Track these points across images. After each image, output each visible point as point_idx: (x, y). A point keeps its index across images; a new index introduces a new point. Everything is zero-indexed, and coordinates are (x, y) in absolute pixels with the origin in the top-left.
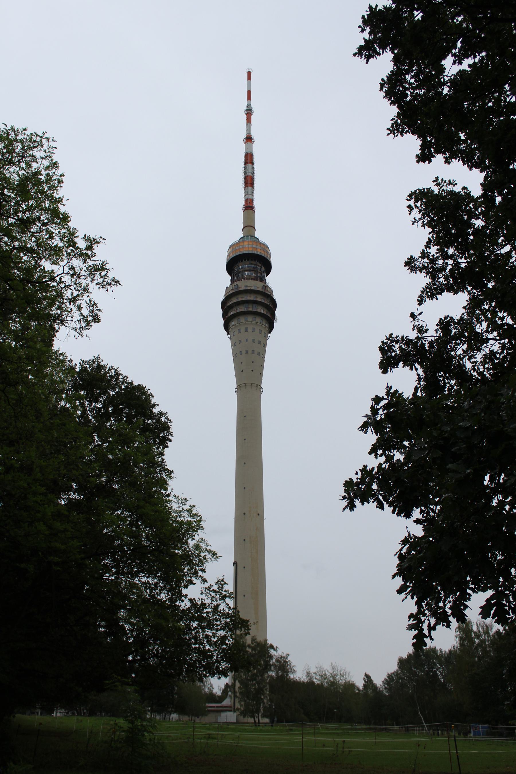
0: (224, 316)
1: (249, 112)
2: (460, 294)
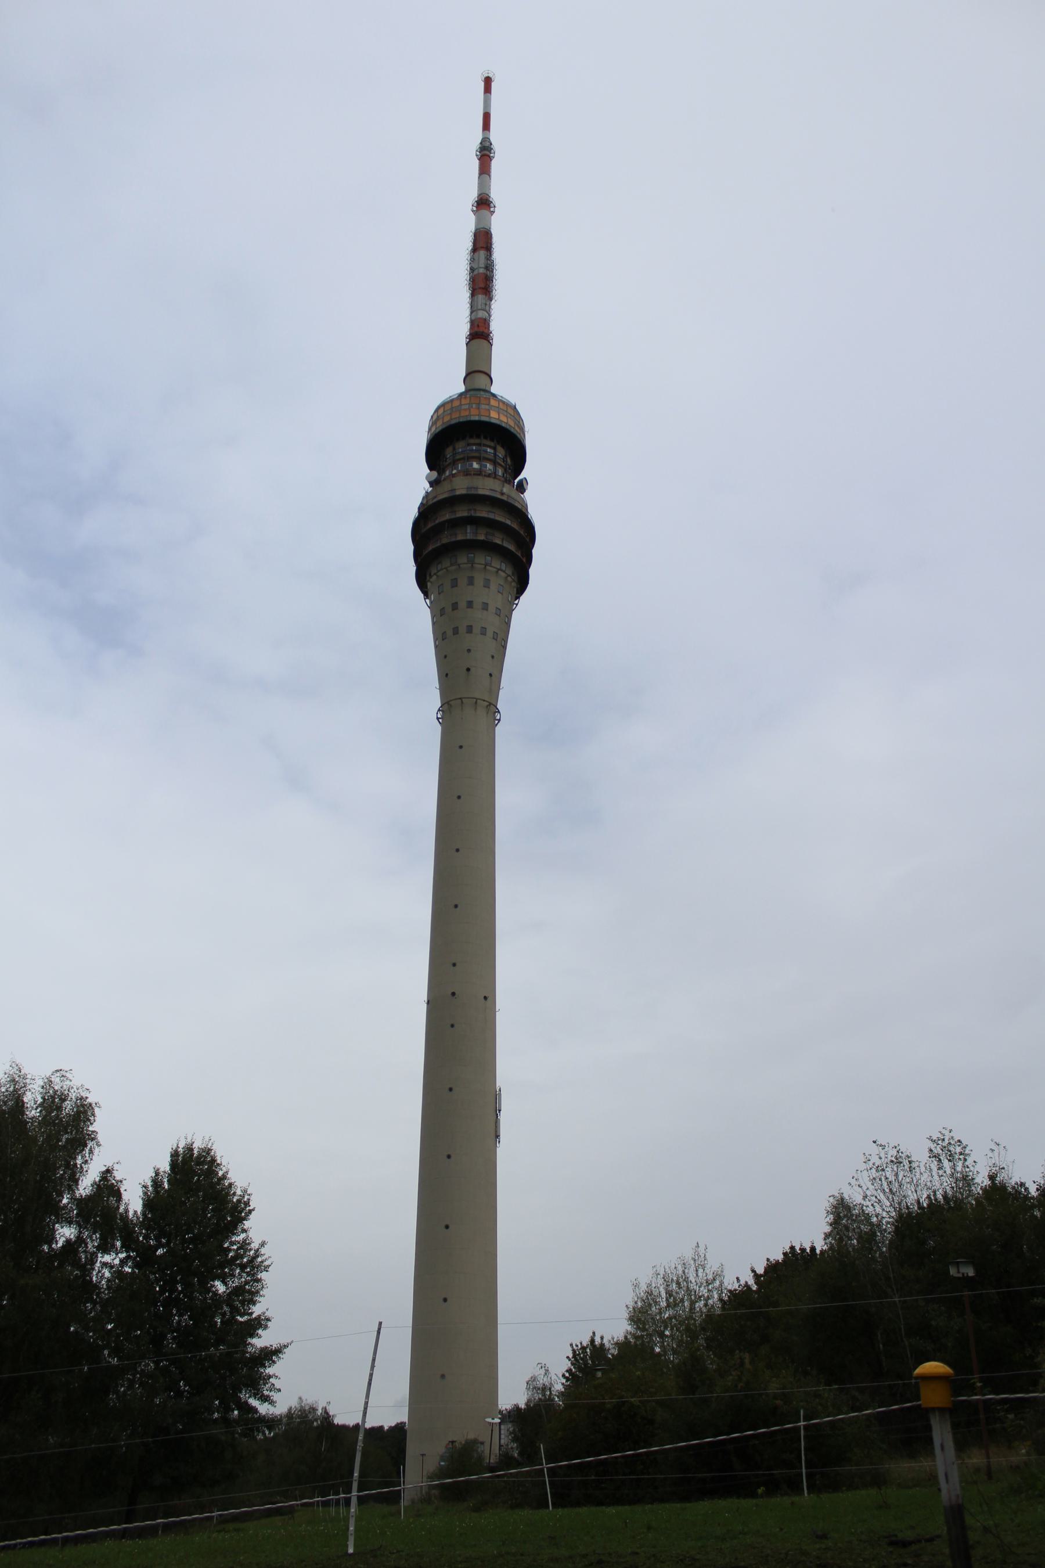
0: (417, 555)
1: (485, 153)
2: (509, 1407)
